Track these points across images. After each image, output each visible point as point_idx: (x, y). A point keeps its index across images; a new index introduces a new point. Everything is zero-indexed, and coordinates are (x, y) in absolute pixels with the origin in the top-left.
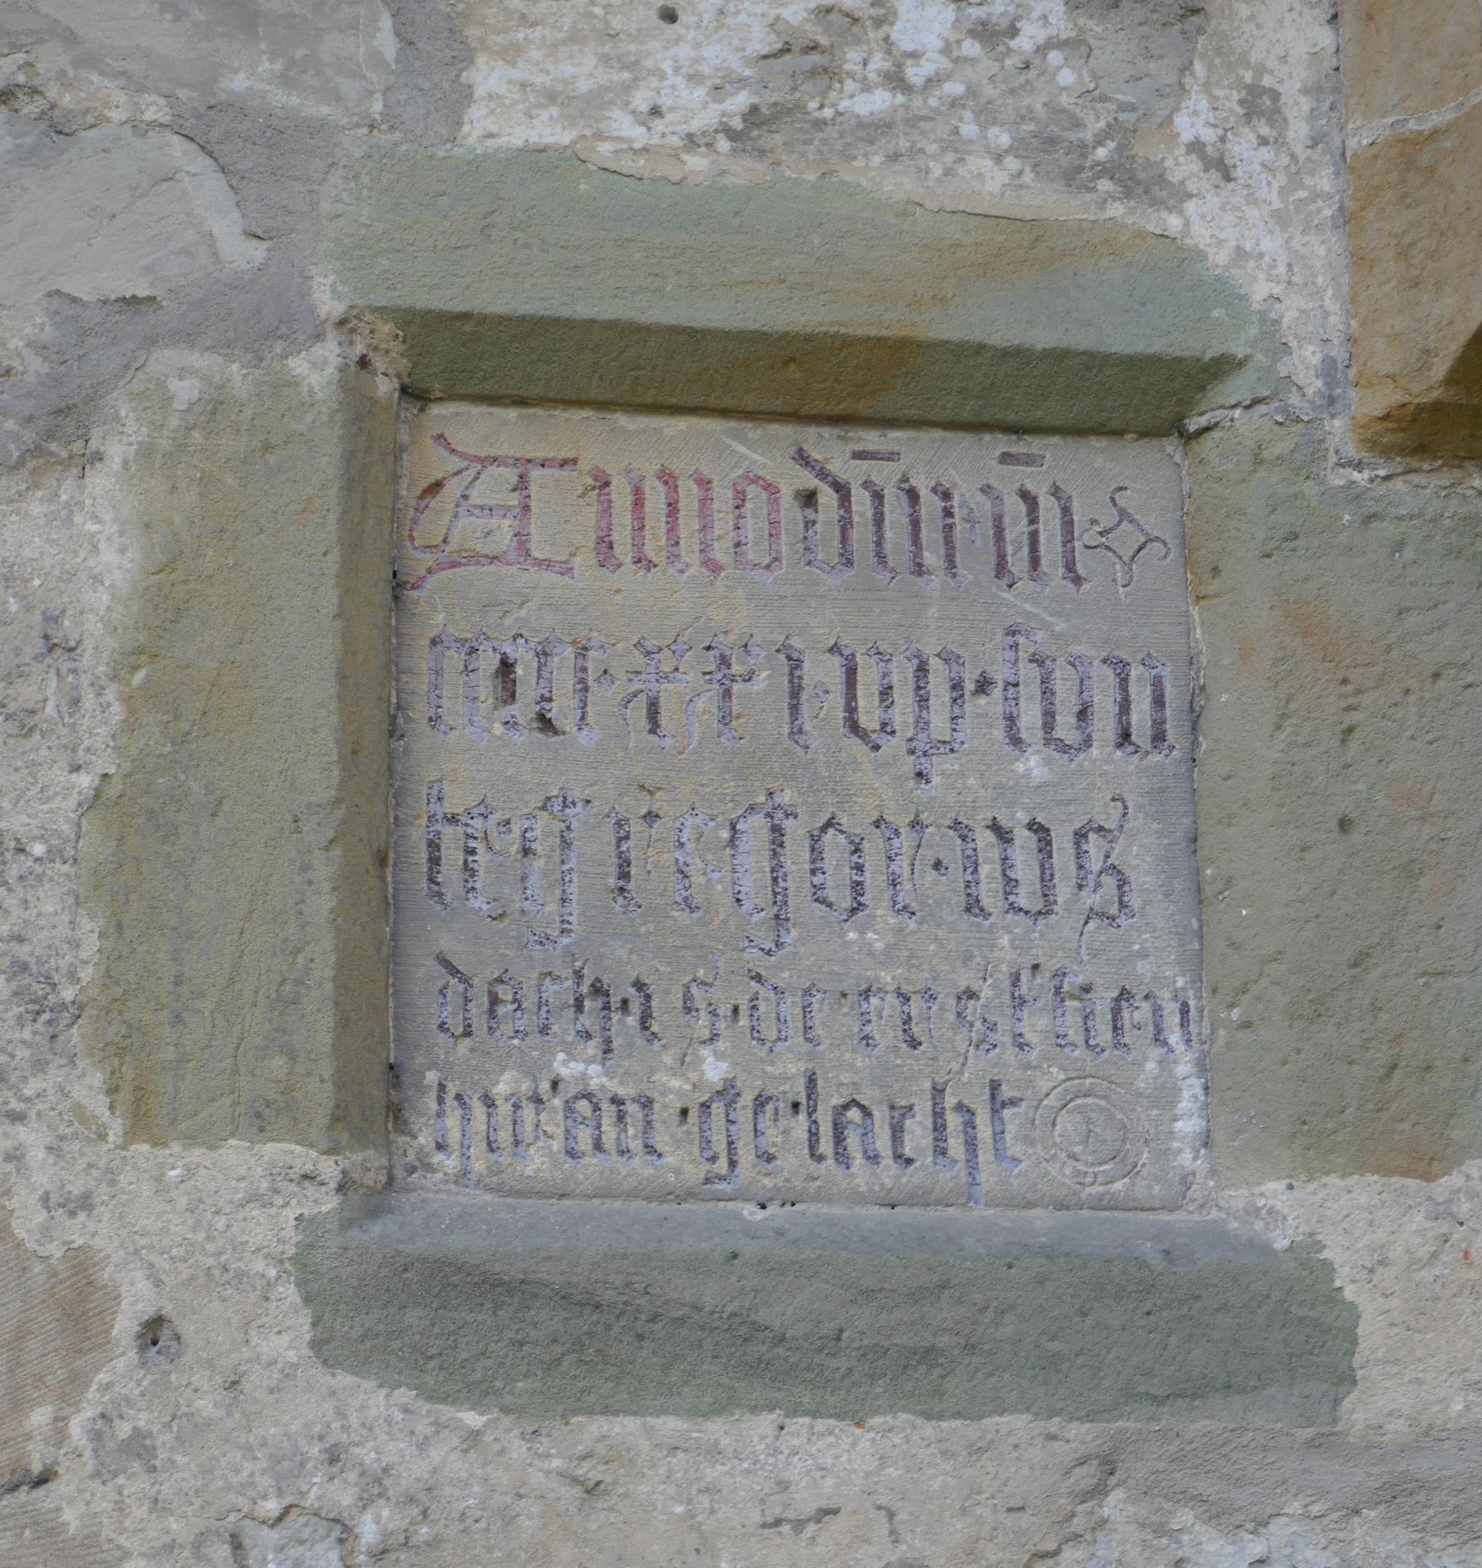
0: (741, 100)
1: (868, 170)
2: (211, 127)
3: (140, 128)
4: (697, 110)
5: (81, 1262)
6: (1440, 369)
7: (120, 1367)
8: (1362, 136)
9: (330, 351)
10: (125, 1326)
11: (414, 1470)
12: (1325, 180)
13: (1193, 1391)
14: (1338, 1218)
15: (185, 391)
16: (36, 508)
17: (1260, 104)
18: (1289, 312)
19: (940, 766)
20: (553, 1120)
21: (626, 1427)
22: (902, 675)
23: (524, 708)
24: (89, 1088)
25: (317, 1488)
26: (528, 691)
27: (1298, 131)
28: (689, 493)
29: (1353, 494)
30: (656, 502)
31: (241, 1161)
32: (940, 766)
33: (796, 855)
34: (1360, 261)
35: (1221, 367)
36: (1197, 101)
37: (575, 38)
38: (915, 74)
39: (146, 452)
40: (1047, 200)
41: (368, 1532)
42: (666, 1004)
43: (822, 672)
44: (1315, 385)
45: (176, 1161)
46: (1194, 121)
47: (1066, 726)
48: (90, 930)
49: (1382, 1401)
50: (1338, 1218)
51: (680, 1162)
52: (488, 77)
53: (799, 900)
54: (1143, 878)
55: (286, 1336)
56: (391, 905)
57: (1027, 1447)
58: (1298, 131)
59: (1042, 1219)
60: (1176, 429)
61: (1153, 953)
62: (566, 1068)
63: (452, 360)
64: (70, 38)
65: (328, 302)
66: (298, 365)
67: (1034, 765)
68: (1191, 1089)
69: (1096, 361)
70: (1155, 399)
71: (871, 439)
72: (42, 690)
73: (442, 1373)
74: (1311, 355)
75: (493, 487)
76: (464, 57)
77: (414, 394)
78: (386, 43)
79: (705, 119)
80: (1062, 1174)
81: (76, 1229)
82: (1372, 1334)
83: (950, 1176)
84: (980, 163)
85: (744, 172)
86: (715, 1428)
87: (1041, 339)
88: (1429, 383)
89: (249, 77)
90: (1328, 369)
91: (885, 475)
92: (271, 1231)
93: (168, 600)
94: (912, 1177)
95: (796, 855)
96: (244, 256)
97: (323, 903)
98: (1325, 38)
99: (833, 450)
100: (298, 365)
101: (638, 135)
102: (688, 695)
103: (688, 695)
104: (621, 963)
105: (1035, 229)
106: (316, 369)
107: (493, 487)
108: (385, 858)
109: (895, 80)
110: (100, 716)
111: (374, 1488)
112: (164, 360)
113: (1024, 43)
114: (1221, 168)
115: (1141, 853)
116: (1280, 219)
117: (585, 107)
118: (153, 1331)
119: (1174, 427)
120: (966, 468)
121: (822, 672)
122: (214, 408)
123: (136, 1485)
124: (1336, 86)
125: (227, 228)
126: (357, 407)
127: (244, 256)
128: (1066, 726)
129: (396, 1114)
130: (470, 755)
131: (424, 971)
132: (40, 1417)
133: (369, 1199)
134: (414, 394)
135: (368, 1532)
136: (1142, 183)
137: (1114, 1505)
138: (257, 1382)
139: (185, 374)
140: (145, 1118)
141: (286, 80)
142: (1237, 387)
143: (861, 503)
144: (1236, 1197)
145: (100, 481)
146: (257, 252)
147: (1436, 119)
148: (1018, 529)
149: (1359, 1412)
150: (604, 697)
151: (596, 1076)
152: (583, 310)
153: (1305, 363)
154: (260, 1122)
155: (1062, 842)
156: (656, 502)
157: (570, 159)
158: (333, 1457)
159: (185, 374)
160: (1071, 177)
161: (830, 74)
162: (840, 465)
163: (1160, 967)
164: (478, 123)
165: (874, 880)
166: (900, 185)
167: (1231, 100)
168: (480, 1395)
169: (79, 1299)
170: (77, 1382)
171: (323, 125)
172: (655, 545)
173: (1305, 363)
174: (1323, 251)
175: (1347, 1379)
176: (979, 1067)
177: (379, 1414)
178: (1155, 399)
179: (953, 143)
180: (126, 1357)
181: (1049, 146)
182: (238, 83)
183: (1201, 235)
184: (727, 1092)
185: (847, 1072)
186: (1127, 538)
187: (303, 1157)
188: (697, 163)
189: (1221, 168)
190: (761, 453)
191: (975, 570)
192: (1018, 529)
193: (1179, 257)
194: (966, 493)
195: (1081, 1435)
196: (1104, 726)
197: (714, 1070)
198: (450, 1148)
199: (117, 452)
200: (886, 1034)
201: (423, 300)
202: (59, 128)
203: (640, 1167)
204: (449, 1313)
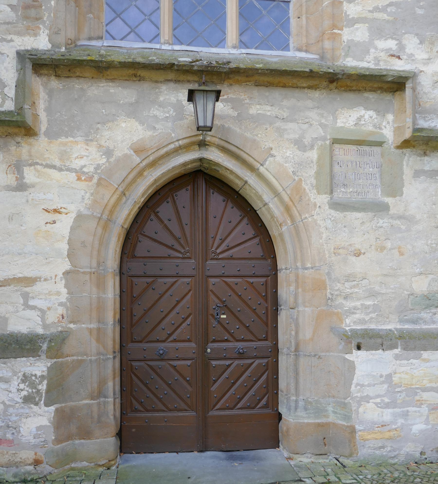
0: (355, 123)
1: (363, 128)
2: (321, 125)
3: (316, 125)
4: (352, 123)
5: (315, 202)
6: (400, 143)
7: (318, 209)
8: (395, 126)
9: (329, 141)
10: (318, 206)
11: (335, 215)
12: (392, 128)
13: (380, 211)
14: (389, 200)
15: (320, 144)
16: (311, 152)
17: (388, 123)
18: (389, 138)
19: (365, 169)
20: (341, 193)
21: (347, 213)
22: (363, 163)
23: (339, 165)
24: (315, 191)
25: (329, 216)
26: (340, 164)
27: (391, 125)
28: (350, 150)
29: (393, 151)
30: (348, 151)
31: (324, 196)
32: (365, 169)
33: (356, 175)
34: (394, 135)
35: (385, 142)
36: (384, 122)
37: (344, 118)
38: (366, 120)
39: (317, 148)
40: (374, 130)
41: (332, 219)
42: (348, 185)
43: (358, 163)
44: (391, 143)
45: (321, 196)
46: (384, 124)
47: (373, 167)
48: (315, 181)
49: (391, 212)
50: (389, 200)
51: (349, 196)
52: (338, 121)
53: (356, 179)
54: (378, 177)
55: (327, 207)
56: (332, 179)
57: (370, 214)
58: (391, 125)
59: (371, 200)
60: (381, 146)
61: (378, 182)
62: (342, 190)
63: (335, 141)
64: (312, 118)
65: (329, 138)
66: (327, 142)
67: (371, 169)
68: (380, 192)
69: (377, 141)
70: (380, 144)
71: (361, 146)
72: (312, 165)
73: (336, 209)
74: (391, 141)
75: (337, 150)
76: (337, 120)
77: (333, 143)
78: (332, 118)
79: (352, 124)
80: (372, 197)
81: (315, 200)
82: (391, 208)
83: (365, 197)
84: (370, 127)
85: (355, 128)
86: (352, 213)
87: (374, 140)
88: (399, 144)
89: (323, 121)
90: (392, 142)
91: (362, 149)
92: (326, 201)
93: (319, 159)
94: (363, 197)
95: (356, 175)
96: (323, 134)
97: (329, 179)
98: (393, 118)
99: (359, 147)
100: (327, 142)
101: (348, 125)
102: (350, 164)
103: (350, 164)
104: (346, 183)
105: (373, 132)
106: (328, 142)
107: (337, 150)
108: (332, 176)
109: (365, 121)
110: (315, 167)
111: (332, 217)
112: (318, 142)
113: (373, 118)
114: (386, 127)
115: (377, 176)
116: (389, 131)
117: (345, 123)
118: (319, 207)
119: (381, 145)
120: (367, 148)
121: (358, 163)
122: (322, 145)
123: (319, 216)
124: (394, 121)
125: (322, 132)
126: (330, 145)
127: (323, 134)
128: (373, 167)
129: (332, 193)
130: (336, 168)
131: (333, 183)
132: (313, 212)
133: (331, 198)
134: (333, 143)
135: (332, 219)
136: (380, 128)
137: (375, 218)
138: (325, 210)
139: (320, 143)
140: (318, 194)
141: (325, 121)
142: (386, 143)
143: (361, 151)
144: (383, 199)
145: (315, 151)
146: (324, 134)
147: (401, 125)
148: (370, 153)
149: (390, 212)
150: (345, 164)
151: (344, 190)
152: (344, 138)
153: (390, 142)
154: (326, 193)
155: (373, 175)
156: (348, 151)
157: (344, 127)
158: (330, 215)
159: (320, 143)
160: (376, 128)
161: (360, 120)
162: (359, 148)
163: (379, 183)
164: (338, 124)
165: (361, 177)
166: (365, 129)
167: (386, 122)
168: (338, 211)
169: (315, 205)
170: (315, 210)
171: (328, 125)
172: (348, 154)
173: (390, 142)
174: (392, 134)
175: (389, 210)
176: (367, 190)
177: (332, 212)
178: (380, 144)
179: (368, 126)
180: (318, 208)
181: (375, 126)
182: (322, 121)
183: (384, 133)
184: (352, 191)
185: (359, 190)
186: (378, 153)
187: (328, 196)
188: (352, 127)
189: (386, 127)
190: (354, 147)
191: (368, 156)
192: (370, 153)
193: (382, 134)
194: (367, 151)
195: (373, 214)
196: (375, 167)
197: (351, 190)
198: (335, 195)
199: (316, 148)
200: (361, 188)
201: (334, 137)
202: (311, 125)
203: (346, 196)
204: (338, 206)
